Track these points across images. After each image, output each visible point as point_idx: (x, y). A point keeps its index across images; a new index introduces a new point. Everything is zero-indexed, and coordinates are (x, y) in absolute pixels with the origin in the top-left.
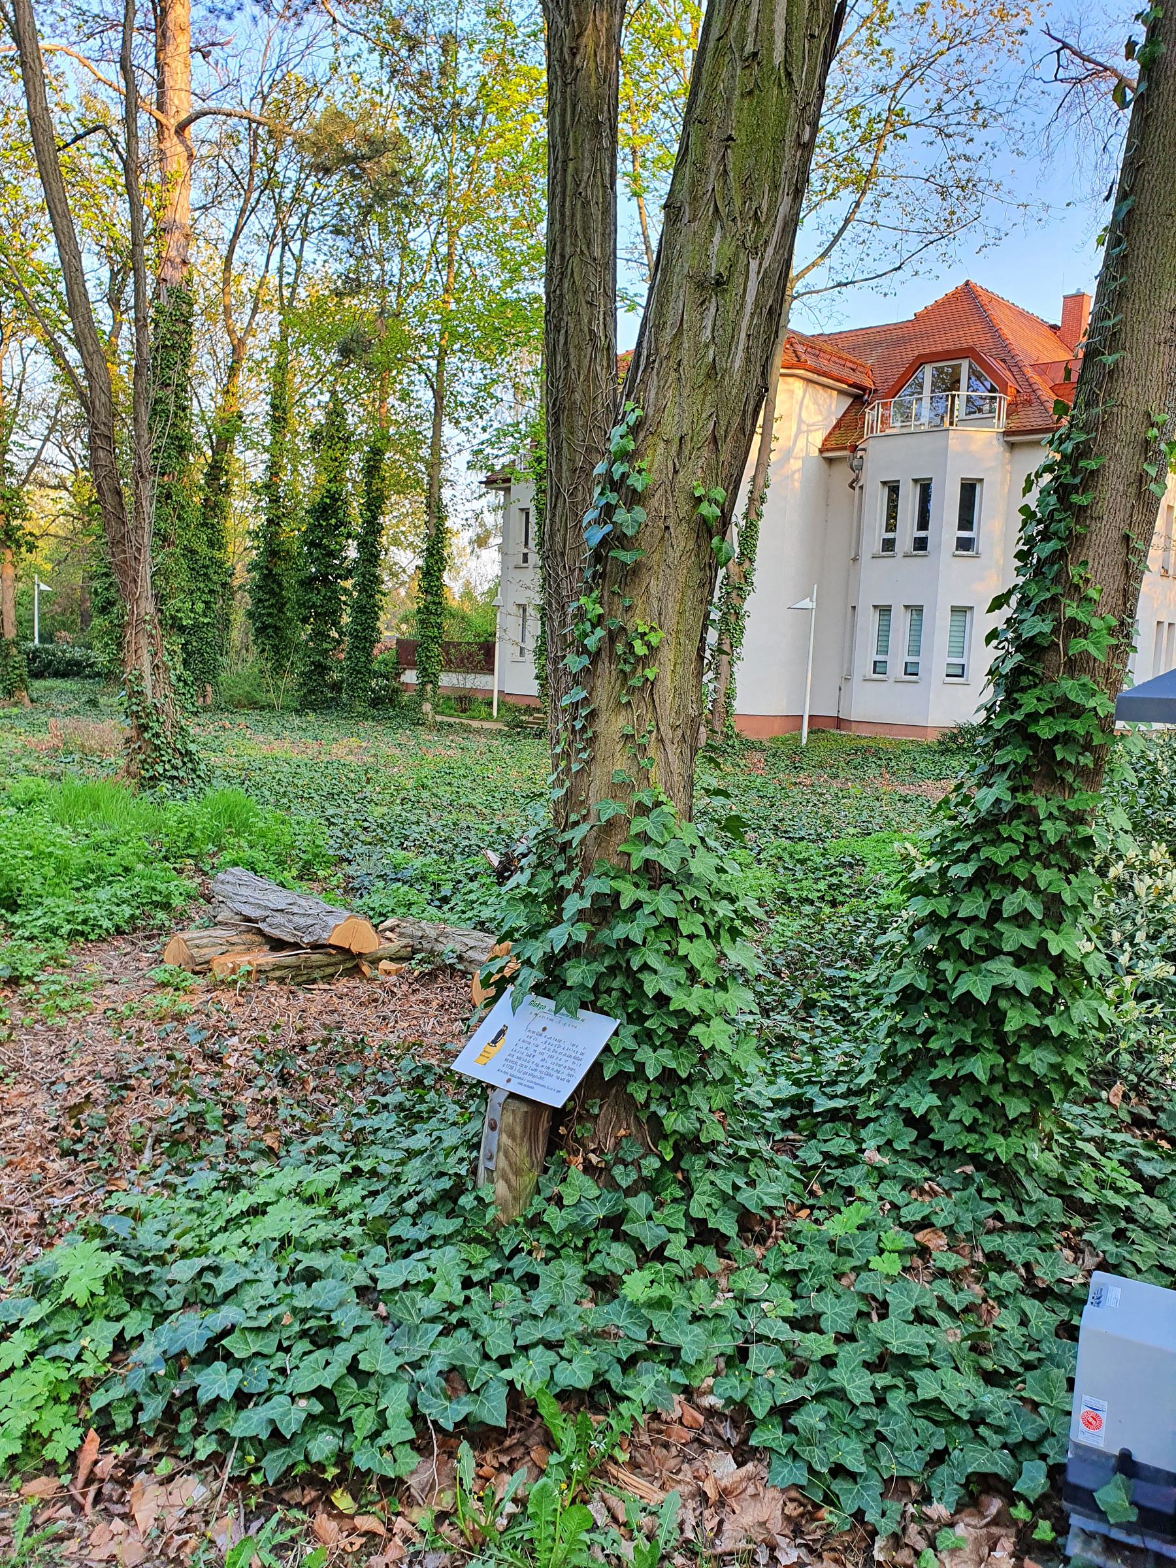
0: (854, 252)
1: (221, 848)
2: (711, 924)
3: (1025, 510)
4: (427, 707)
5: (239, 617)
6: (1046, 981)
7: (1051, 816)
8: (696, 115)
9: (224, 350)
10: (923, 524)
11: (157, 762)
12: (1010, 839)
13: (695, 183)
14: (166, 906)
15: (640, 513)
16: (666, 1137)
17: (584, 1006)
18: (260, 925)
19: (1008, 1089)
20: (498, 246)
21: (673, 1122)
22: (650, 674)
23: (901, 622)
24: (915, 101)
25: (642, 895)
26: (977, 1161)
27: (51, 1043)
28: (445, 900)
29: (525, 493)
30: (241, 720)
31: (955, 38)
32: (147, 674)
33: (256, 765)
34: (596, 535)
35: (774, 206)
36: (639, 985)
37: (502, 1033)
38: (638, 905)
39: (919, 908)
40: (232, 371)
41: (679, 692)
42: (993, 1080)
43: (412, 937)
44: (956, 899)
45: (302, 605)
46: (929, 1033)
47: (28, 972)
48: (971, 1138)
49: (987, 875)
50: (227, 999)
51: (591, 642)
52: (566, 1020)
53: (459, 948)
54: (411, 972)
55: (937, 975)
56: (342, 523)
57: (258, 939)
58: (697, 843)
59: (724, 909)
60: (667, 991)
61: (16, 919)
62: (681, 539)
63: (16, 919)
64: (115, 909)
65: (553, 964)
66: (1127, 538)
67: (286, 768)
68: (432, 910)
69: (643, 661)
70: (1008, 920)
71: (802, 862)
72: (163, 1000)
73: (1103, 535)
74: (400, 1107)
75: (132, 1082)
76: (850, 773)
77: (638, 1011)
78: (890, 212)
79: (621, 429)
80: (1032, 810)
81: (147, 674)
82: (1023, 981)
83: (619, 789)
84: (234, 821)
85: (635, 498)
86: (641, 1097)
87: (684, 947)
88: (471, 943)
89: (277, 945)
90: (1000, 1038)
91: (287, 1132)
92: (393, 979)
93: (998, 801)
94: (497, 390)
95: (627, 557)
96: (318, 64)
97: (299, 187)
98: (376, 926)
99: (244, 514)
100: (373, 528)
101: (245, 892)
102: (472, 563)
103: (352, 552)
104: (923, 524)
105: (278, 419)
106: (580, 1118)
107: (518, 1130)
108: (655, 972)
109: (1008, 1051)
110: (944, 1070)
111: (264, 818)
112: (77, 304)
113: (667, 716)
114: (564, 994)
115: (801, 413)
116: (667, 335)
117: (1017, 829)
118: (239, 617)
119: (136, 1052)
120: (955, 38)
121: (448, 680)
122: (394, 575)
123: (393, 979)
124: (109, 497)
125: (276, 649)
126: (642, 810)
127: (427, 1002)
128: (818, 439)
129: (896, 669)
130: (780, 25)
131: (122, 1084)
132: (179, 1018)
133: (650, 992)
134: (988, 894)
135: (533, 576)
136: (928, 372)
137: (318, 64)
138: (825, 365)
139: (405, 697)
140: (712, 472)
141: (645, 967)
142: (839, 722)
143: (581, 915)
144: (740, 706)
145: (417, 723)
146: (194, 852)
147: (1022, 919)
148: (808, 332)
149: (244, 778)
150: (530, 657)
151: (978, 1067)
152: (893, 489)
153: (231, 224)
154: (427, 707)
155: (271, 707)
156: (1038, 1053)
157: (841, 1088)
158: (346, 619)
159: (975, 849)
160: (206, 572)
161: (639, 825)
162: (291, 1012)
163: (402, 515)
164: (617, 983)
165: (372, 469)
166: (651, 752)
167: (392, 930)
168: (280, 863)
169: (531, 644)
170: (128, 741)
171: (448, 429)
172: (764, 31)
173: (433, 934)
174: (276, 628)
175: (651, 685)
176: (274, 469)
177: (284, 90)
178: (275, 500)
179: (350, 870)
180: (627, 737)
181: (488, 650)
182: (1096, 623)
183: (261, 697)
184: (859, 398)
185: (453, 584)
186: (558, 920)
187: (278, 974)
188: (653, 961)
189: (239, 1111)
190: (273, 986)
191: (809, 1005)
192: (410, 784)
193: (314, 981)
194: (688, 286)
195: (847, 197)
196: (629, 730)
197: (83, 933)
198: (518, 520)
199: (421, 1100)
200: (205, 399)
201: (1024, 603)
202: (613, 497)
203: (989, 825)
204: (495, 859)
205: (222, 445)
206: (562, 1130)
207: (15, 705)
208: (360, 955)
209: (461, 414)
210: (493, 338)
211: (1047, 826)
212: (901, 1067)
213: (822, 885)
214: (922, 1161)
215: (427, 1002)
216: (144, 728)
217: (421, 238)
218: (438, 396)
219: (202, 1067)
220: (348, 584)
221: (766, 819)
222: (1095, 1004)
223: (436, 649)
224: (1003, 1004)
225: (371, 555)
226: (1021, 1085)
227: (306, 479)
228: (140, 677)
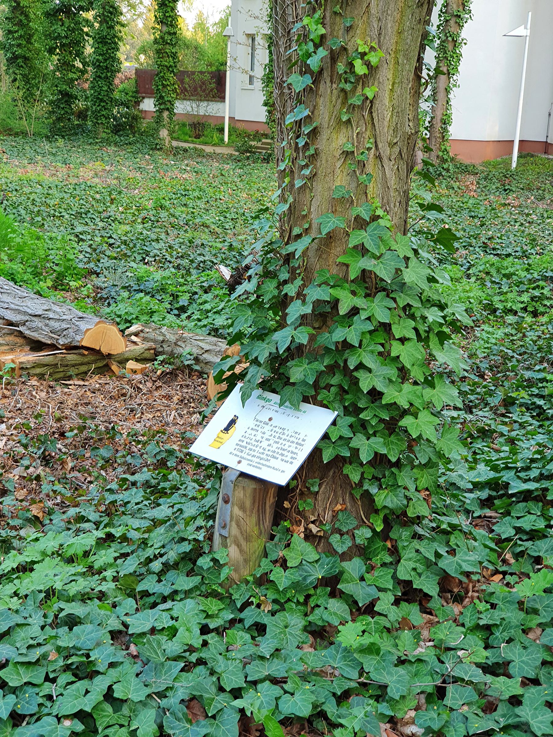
2: (422, 328)
4: (164, 133)
17: (306, 400)
18: (21, 328)
21: (384, 499)
22: (369, 93)
25: (359, 302)
28: (183, 309)
33: (13, 186)
36: (355, 382)
38: (355, 311)
43: (155, 341)
51: (314, 62)
53: (195, 351)
54: (154, 371)
57: (19, 340)
59: (433, 315)
67: (39, 189)
68: (171, 318)
69: (363, 80)
71: (508, 276)
74: (147, 484)
83: (340, 203)
87: (396, 349)
89: (37, 346)
91: (50, 504)
92: (139, 377)
98: (123, 331)
121: (182, 107)
123: (139, 377)
125: (26, 79)
126: (361, 224)
133: (365, 387)
139: (144, 125)
141: (361, 366)
143: (304, 320)
144: (455, 132)
145: (156, 148)
150: (258, 84)
154: (164, 133)
155: (24, 134)
158: (89, 50)
161: (357, 237)
164: (334, 381)
166: (370, 168)
167: (136, 334)
169: (260, 72)
173: (172, 338)
175: (370, 104)
179: (99, 281)
180: (347, 154)
183: (15, 124)
186: (282, 325)
187: (38, 371)
188: (369, 362)
191: (508, 403)
192: (150, 204)
193: (70, 378)
196: (349, 147)
204: (227, 273)
208: (109, 356)
213: (525, 298)
215: (169, 397)
220: (90, 15)
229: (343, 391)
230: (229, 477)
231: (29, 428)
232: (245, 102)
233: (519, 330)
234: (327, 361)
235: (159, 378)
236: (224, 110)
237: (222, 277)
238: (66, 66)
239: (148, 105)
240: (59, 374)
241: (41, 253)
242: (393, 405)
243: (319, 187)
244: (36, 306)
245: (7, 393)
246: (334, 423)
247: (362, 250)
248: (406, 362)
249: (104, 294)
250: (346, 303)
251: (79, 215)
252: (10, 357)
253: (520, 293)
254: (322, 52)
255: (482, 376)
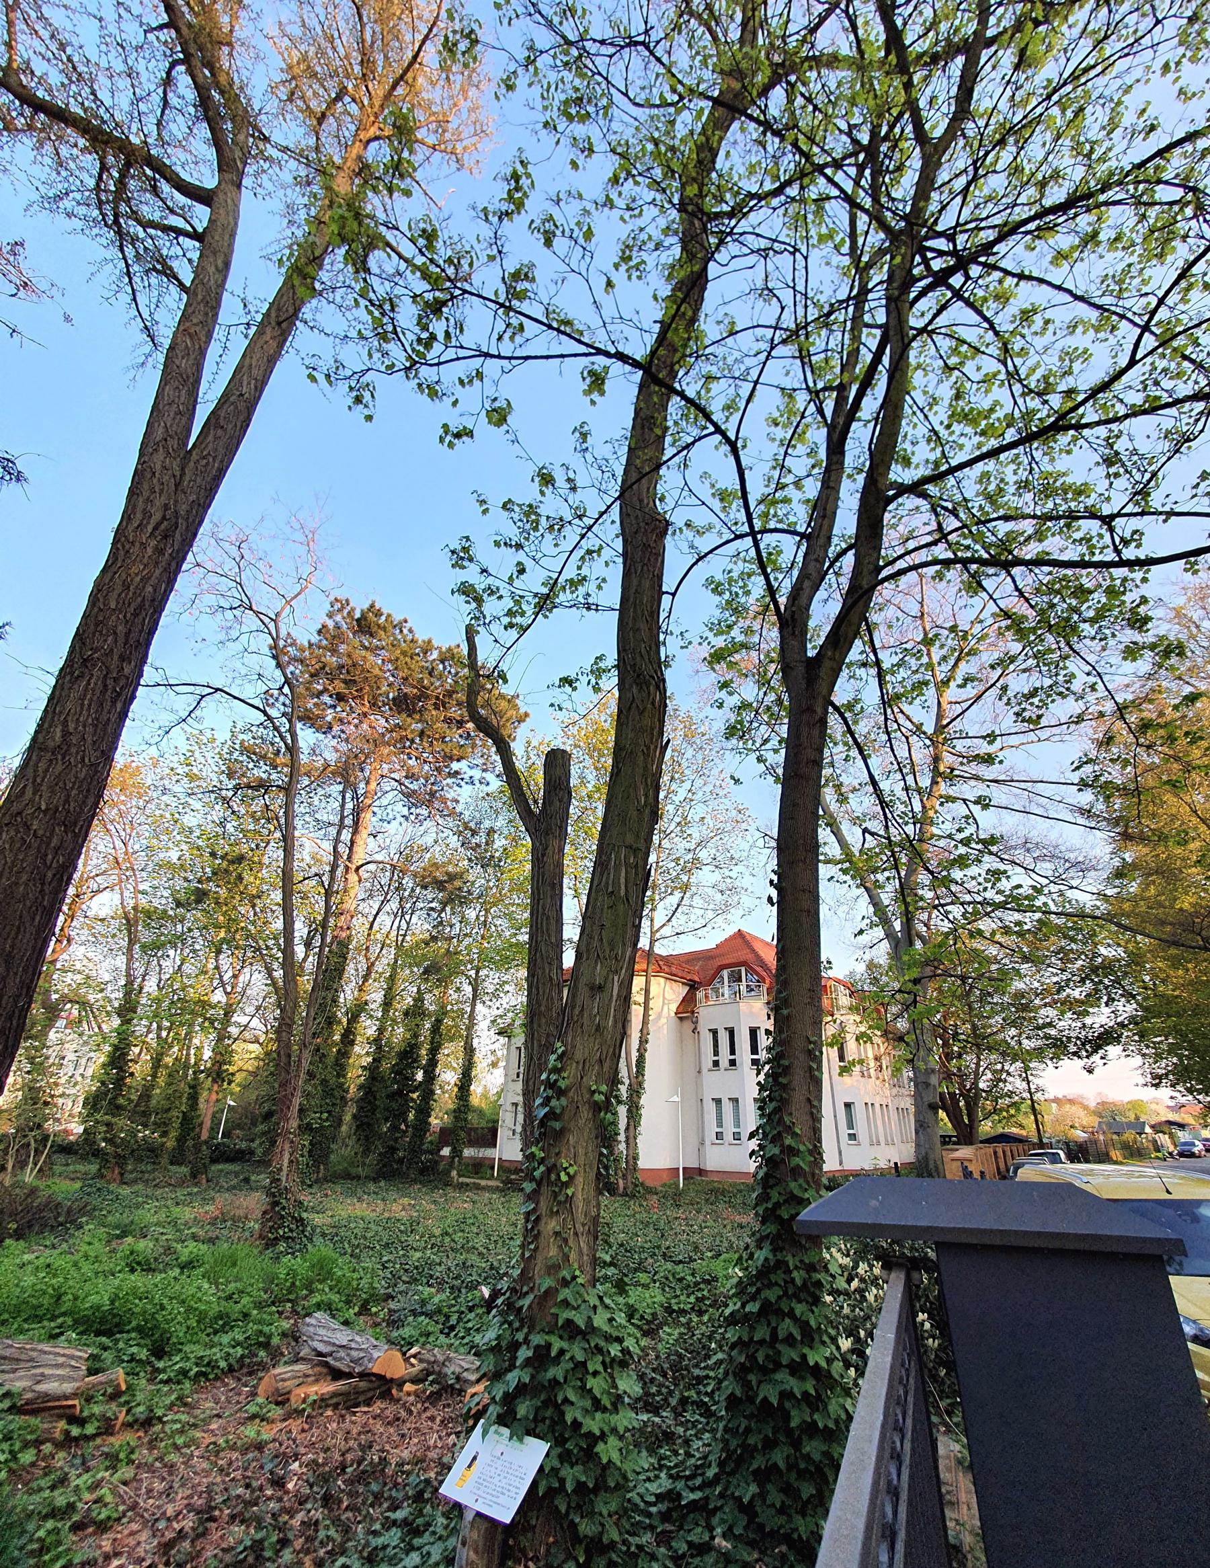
0: (683, 918)
1: (311, 1292)
2: (608, 1360)
3: (759, 1083)
4: (454, 1173)
5: (348, 1118)
6: (810, 1387)
7: (796, 1268)
8: (601, 865)
9: (363, 966)
10: (733, 1052)
11: (282, 1227)
12: (776, 1284)
13: (588, 944)
14: (266, 1345)
15: (564, 1101)
16: (580, 1542)
17: (528, 1434)
18: (329, 1359)
19: (802, 1474)
20: (509, 916)
21: (586, 1528)
22: (569, 1192)
23: (727, 1107)
24: (703, 855)
25: (565, 1345)
26: (787, 1539)
27: (163, 1479)
28: (452, 1328)
29: (520, 1040)
30: (338, 1188)
31: (719, 832)
32: (285, 1168)
33: (344, 1223)
34: (542, 1112)
35: (624, 953)
36: (562, 1414)
37: (475, 1458)
38: (562, 1352)
39: (732, 1335)
40: (366, 978)
41: (587, 1201)
42: (790, 1467)
43: (429, 1362)
44: (752, 1328)
45: (387, 1109)
46: (748, 1430)
47: (159, 1413)
48: (782, 1520)
49: (767, 1309)
50: (295, 1425)
51: (537, 1174)
52: (517, 1444)
53: (458, 1370)
54: (424, 1391)
55: (747, 1385)
56: (415, 1061)
57: (325, 1370)
58: (598, 1303)
59: (615, 1350)
60: (580, 1419)
61: (161, 1365)
62: (585, 1113)
63: (161, 1365)
64: (231, 1351)
65: (509, 1399)
66: (809, 1100)
67: (362, 1224)
68: (442, 1338)
69: (566, 1185)
70: (782, 1341)
71: (681, 1280)
72: (250, 1432)
73: (798, 1098)
74: (406, 1522)
75: (217, 1513)
76: (707, 1208)
77: (562, 1435)
78: (697, 901)
79: (553, 1057)
80: (787, 1263)
81: (285, 1168)
82: (795, 1386)
83: (552, 1269)
84: (323, 1271)
85: (561, 1093)
86: (563, 1509)
87: (591, 1382)
88: (466, 1366)
89: (337, 1375)
90: (789, 1432)
91: (322, 1552)
92: (412, 1398)
93: (766, 1259)
94: (507, 988)
95: (557, 1125)
96: (429, 840)
97: (413, 890)
98: (404, 1354)
99: (362, 1054)
100: (433, 1063)
101: (324, 1332)
102: (489, 1077)
103: (420, 1076)
104: (733, 1052)
105: (387, 1004)
106: (525, 1530)
107: (481, 1544)
108: (572, 1404)
109: (796, 1444)
110: (758, 1462)
111: (342, 1268)
112: (288, 951)
113: (580, 1217)
114: (516, 1424)
115: (660, 997)
116: (577, 1011)
117: (778, 1277)
118: (348, 1118)
119: (224, 1482)
120: (719, 832)
121: (468, 1152)
122: (441, 1087)
123: (412, 1398)
124: (283, 1058)
125: (367, 1138)
126: (565, 1283)
127: (432, 1419)
128: (674, 1007)
129: (729, 1137)
130: (623, 880)
131: (207, 1515)
132: (259, 1447)
133: (569, 1419)
134: (769, 1324)
135: (519, 1086)
136: (725, 973)
137: (429, 840)
138: (674, 970)
139: (441, 1167)
140: (599, 1078)
141: (566, 1400)
142: (701, 1172)
143: (528, 1362)
144: (642, 1164)
145: (447, 1184)
146: (291, 1297)
147: (790, 1340)
148: (664, 954)
149: (334, 1236)
150: (518, 1137)
151: (779, 1457)
152: (714, 1032)
153: (376, 907)
154: (454, 1173)
155: (358, 1177)
156: (814, 1443)
157: (698, 1481)
158: (411, 1116)
159: (758, 1291)
160: (333, 1093)
161: (565, 1293)
162: (337, 1432)
163: (451, 1053)
164: (548, 1413)
165: (436, 1029)
166: (571, 1243)
167: (414, 1356)
168: (348, 1302)
169: (519, 1129)
170: (265, 1213)
171: (479, 1007)
172: (616, 882)
173: (441, 1358)
174: (369, 1124)
175: (570, 1199)
176: (381, 1030)
177: (408, 853)
178: (379, 1048)
179: (392, 1305)
180: (557, 1234)
181: (494, 1132)
182: (802, 1148)
183: (353, 1171)
184: (693, 987)
185: (476, 1089)
186: (512, 1367)
187: (334, 1400)
188: (572, 1397)
189: (290, 1535)
190: (329, 1413)
191: (684, 1401)
192: (437, 1232)
193: (357, 1405)
194: (586, 989)
195: (678, 895)
196: (558, 1228)
197: (207, 1374)
198: (515, 1053)
199: (420, 1513)
200: (348, 995)
201: (765, 1135)
202: (550, 1092)
203: (764, 1273)
204: (486, 1292)
205: (354, 1018)
206: (511, 1542)
207: (196, 1185)
208: (392, 1380)
209: (486, 998)
210: (504, 963)
211: (795, 1274)
212: (733, 1463)
213: (692, 1299)
214: (752, 1544)
215: (432, 1419)
216: (277, 1203)
217: (471, 914)
218: (475, 990)
219: (269, 1493)
220: (415, 1096)
221: (659, 1247)
222: (841, 1400)
223: (463, 1134)
224: (787, 1405)
225: (430, 1077)
226: (806, 1470)
227: (398, 1034)
228: (280, 1170)
229: (554, 1423)
230: (469, 1516)
231: (318, 1465)
232: (509, 1148)
233: (689, 1329)
234: (543, 1397)
235: (428, 1397)
236: (495, 1153)
237: (483, 1297)
238: (395, 1128)
239: (446, 1151)
240: (347, 1402)
241: (355, 1283)
242: (590, 1434)
243: (540, 1260)
244: (342, 1336)
245: (306, 1427)
246: (547, 1455)
247: (566, 1303)
248: (597, 1392)
249: (395, 1317)
250: (557, 1344)
251: (387, 1245)
252: (315, 1388)
253: (688, 1296)
254: (542, 1168)
255: (665, 1376)
